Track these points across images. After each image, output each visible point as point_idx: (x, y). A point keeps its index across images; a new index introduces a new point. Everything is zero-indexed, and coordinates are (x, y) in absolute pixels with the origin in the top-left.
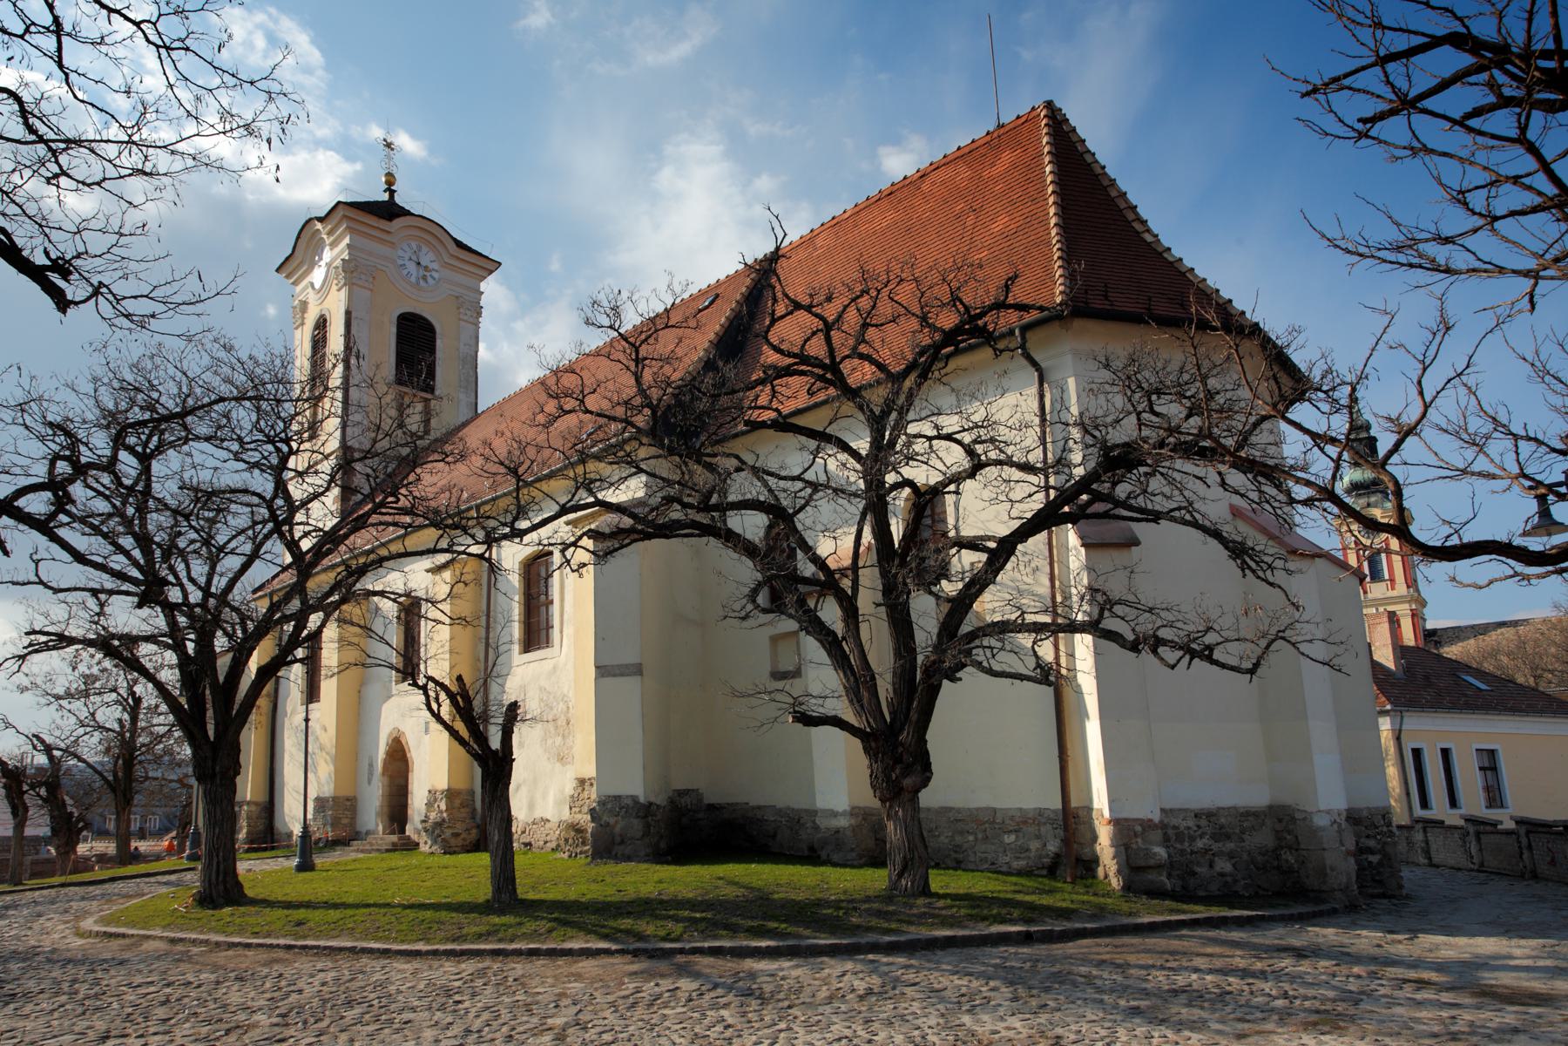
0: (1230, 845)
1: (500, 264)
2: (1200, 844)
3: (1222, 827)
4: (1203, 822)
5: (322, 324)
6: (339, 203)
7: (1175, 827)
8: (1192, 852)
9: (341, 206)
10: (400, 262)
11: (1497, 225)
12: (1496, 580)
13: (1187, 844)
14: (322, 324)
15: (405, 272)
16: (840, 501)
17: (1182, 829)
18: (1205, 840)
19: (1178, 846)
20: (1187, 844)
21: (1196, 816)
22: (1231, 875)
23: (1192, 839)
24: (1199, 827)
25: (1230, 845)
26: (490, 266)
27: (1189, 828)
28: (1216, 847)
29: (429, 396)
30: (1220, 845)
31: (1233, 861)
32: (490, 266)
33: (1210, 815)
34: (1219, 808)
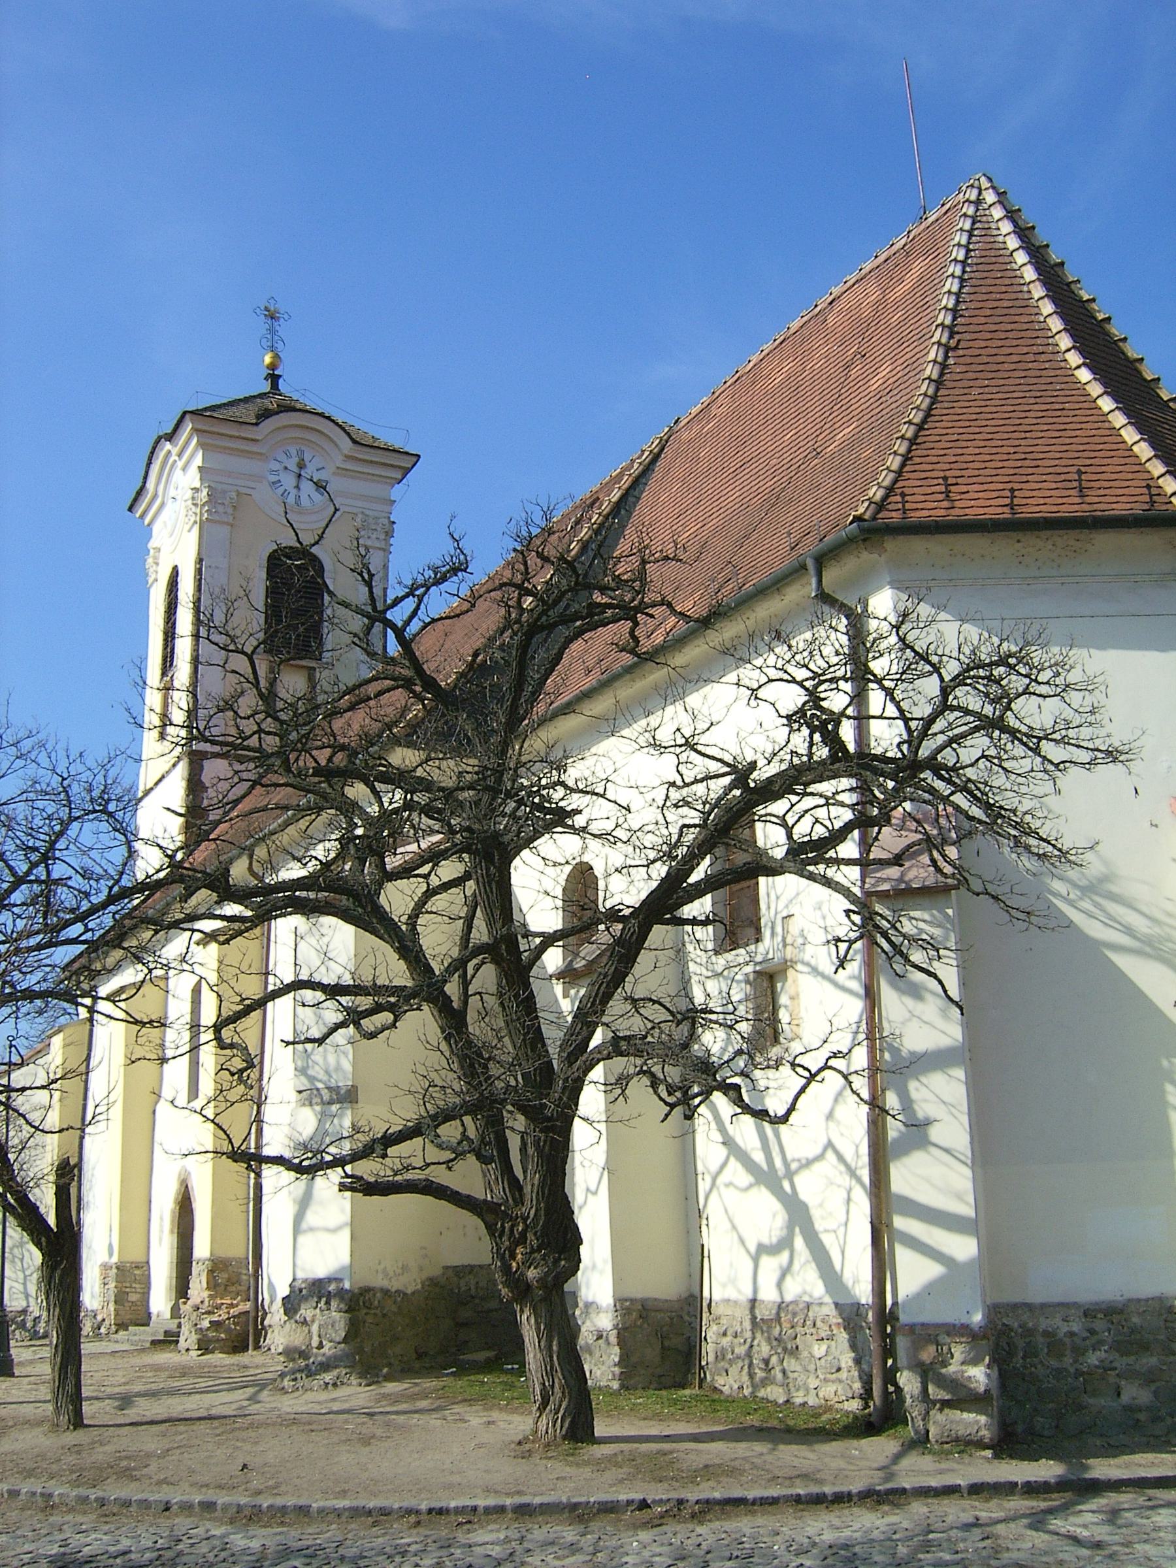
0: (1151, 1361)
1: (419, 456)
2: (1093, 1359)
3: (1133, 1331)
4: (1100, 1325)
5: (175, 572)
6: (185, 413)
7: (1046, 1333)
8: (1079, 1373)
9: (188, 416)
10: (274, 478)
11: (760, 694)
12: (328, 1230)
13: (1068, 1360)
14: (175, 572)
15: (281, 490)
16: (968, 743)
17: (1061, 1334)
18: (1101, 1354)
19: (1054, 1363)
20: (1068, 1360)
21: (1086, 1314)
22: (1148, 1409)
23: (1079, 1352)
24: (1092, 1332)
25: (1151, 1361)
26: (406, 462)
27: (1072, 1334)
28: (1121, 1362)
29: (313, 664)
30: (1131, 1359)
31: (1153, 1387)
32: (406, 462)
33: (1112, 1312)
34: (1129, 1300)
